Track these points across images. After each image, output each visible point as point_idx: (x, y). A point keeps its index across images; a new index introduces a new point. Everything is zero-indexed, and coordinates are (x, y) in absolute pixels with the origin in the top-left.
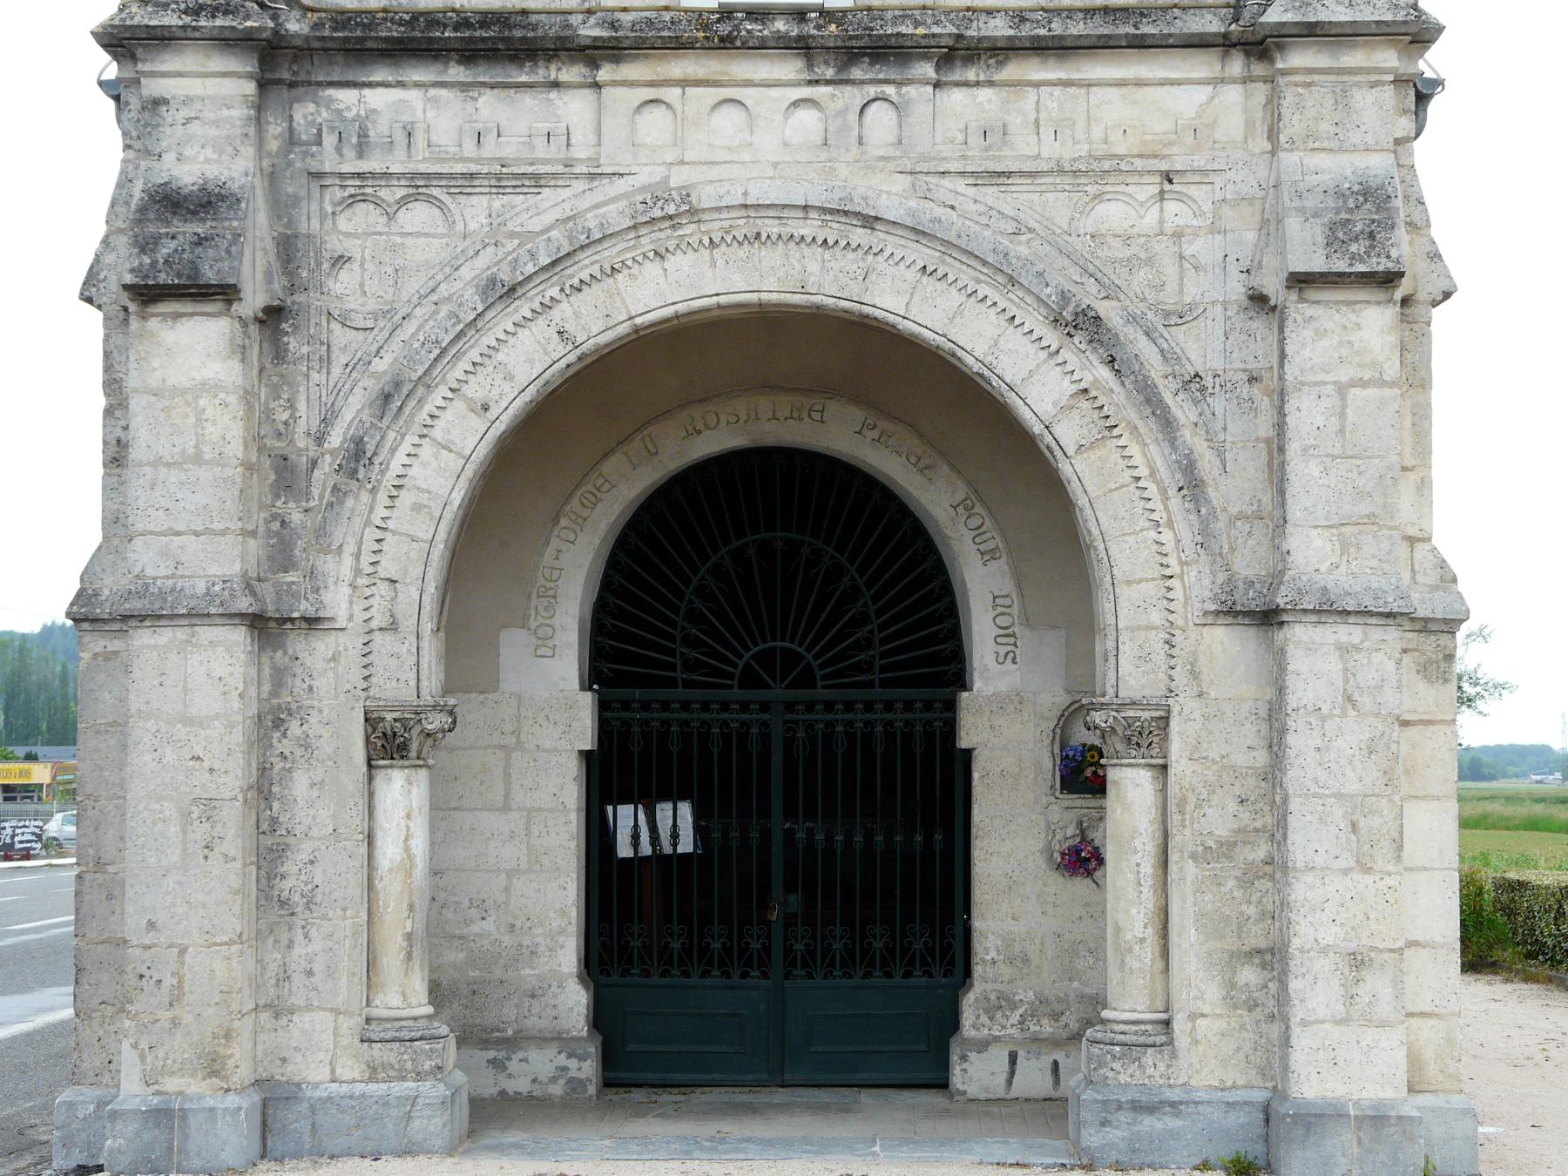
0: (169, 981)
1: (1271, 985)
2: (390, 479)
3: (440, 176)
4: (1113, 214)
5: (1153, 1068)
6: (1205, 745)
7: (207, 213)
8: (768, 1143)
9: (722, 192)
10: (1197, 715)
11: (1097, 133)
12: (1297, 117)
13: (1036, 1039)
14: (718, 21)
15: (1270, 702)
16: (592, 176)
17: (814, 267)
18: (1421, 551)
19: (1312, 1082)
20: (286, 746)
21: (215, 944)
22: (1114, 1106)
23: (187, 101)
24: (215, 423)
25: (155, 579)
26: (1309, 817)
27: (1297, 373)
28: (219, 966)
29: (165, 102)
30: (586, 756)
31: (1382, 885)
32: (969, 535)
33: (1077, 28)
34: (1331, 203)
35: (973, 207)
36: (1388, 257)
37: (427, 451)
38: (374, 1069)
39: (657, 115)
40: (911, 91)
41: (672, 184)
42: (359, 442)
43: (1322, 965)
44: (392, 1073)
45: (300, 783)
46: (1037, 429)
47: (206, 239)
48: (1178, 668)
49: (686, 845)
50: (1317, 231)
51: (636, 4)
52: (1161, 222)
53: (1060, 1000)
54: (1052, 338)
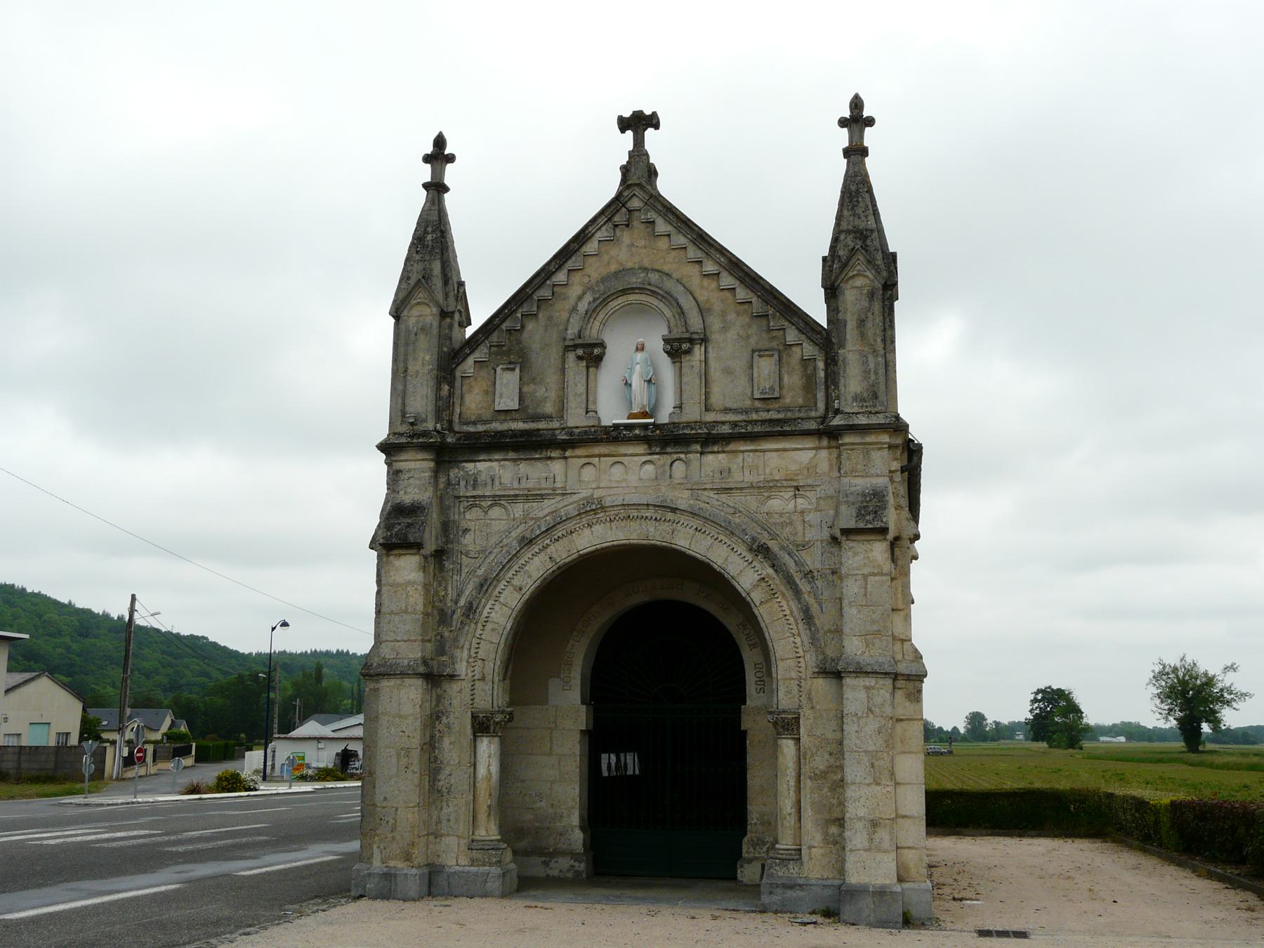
0: (392, 821)
2: (483, 618)
4: (775, 504)
5: (793, 869)
8: (637, 899)
11: (767, 471)
16: (563, 494)
17: (652, 529)
18: (906, 645)
19: (855, 877)
20: (441, 727)
23: (409, 470)
28: (410, 816)
33: (758, 429)
34: (860, 498)
37: (497, 607)
39: (588, 469)
40: (691, 456)
42: (471, 603)
43: (859, 825)
45: (446, 743)
50: (854, 512)
54: (749, 557)
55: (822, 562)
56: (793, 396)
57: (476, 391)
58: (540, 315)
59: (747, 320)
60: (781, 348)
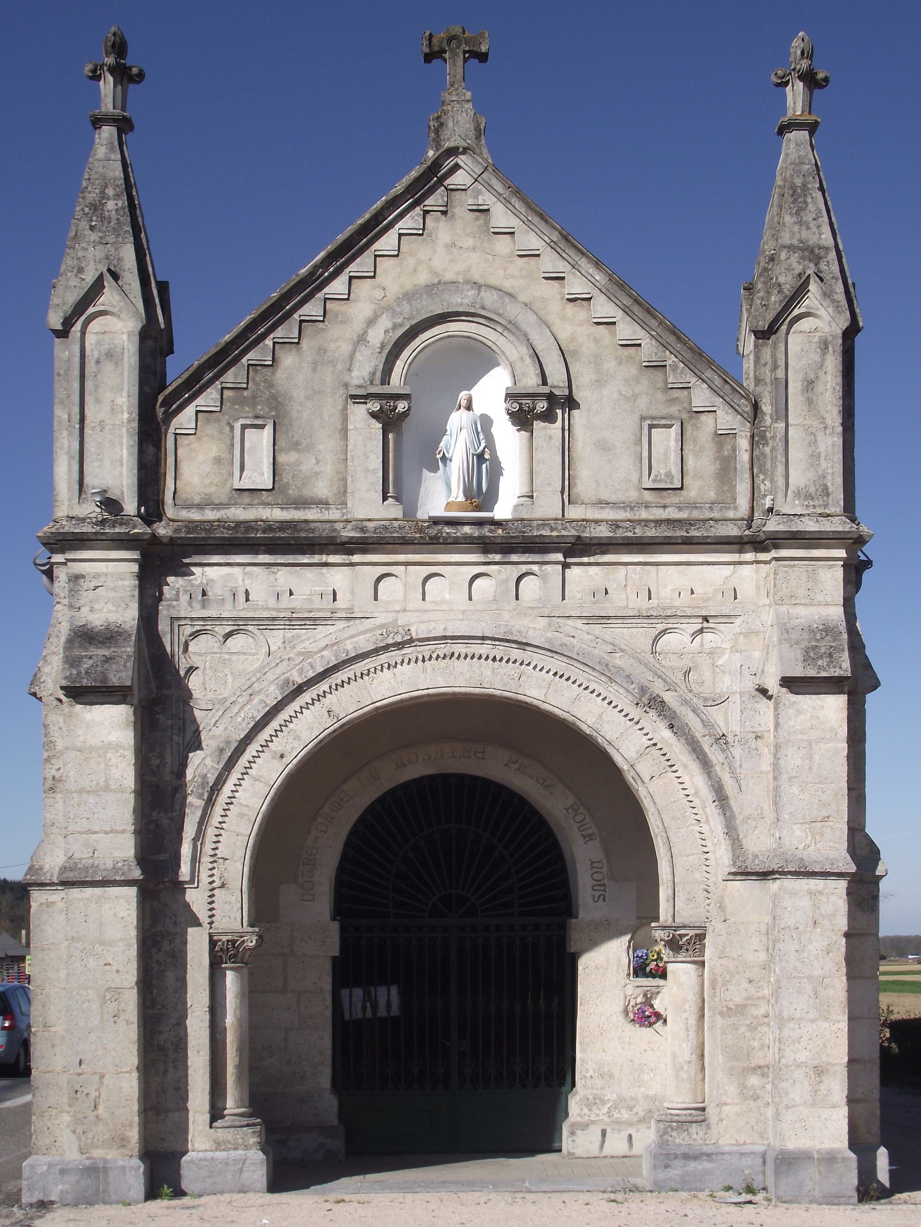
1: (767, 1086)
3: (253, 619)
6: (728, 949)
7: (110, 643)
9: (431, 628)
10: (723, 932)
12: (785, 585)
13: (618, 1122)
14: (428, 527)
15: (767, 924)
16: (348, 619)
17: (488, 673)
21: (122, 1072)
22: (673, 1157)
23: (96, 576)
24: (117, 767)
25: (81, 859)
26: (791, 990)
27: (786, 735)
29: (83, 577)
30: (334, 959)
31: (834, 1028)
32: (575, 826)
33: (651, 532)
35: (587, 637)
36: (841, 668)
38: (219, 1144)
41: (399, 623)
43: (799, 1074)
44: (229, 1146)
46: (624, 767)
47: (111, 659)
48: (712, 905)
49: (395, 1011)
51: (376, 517)
52: (702, 645)
53: (632, 1099)
54: (635, 713)
55: (742, 723)
56: (701, 487)
57: (201, 457)
58: (304, 344)
59: (634, 371)
60: (685, 416)
